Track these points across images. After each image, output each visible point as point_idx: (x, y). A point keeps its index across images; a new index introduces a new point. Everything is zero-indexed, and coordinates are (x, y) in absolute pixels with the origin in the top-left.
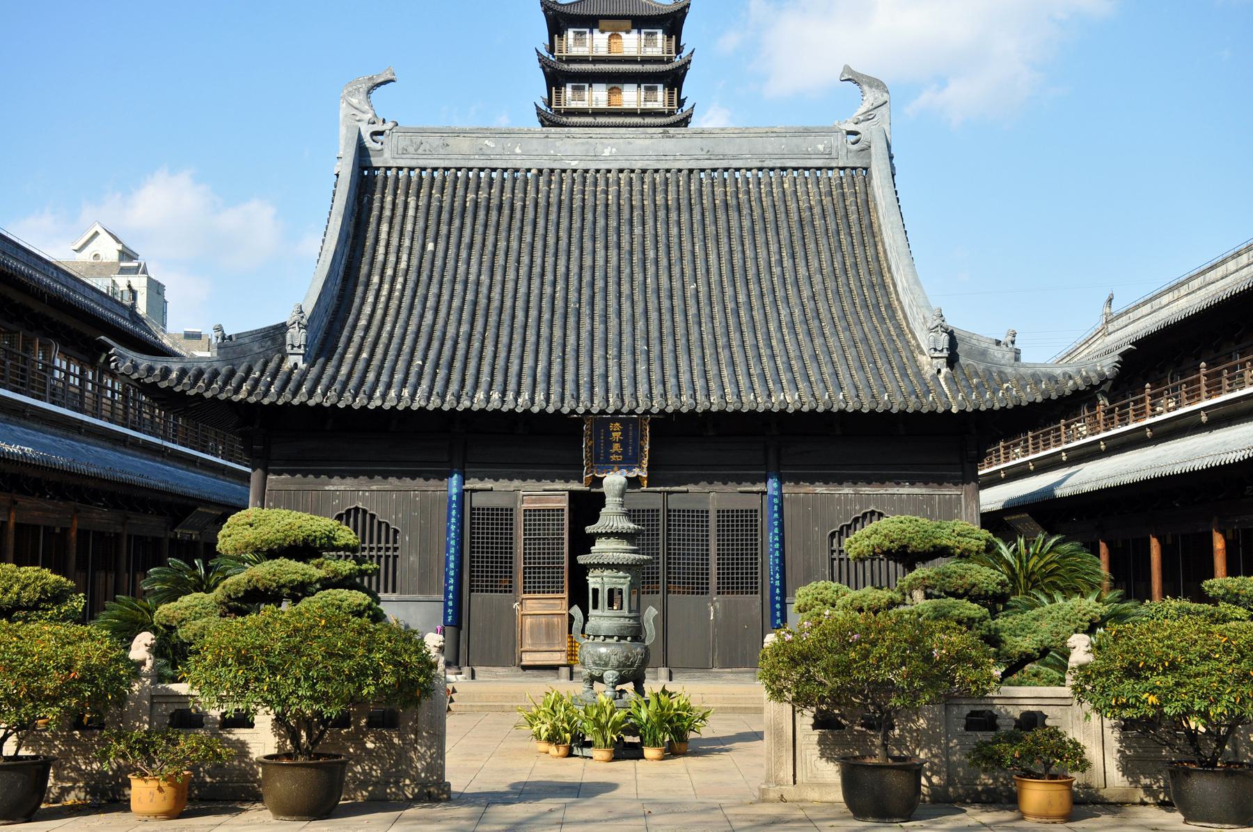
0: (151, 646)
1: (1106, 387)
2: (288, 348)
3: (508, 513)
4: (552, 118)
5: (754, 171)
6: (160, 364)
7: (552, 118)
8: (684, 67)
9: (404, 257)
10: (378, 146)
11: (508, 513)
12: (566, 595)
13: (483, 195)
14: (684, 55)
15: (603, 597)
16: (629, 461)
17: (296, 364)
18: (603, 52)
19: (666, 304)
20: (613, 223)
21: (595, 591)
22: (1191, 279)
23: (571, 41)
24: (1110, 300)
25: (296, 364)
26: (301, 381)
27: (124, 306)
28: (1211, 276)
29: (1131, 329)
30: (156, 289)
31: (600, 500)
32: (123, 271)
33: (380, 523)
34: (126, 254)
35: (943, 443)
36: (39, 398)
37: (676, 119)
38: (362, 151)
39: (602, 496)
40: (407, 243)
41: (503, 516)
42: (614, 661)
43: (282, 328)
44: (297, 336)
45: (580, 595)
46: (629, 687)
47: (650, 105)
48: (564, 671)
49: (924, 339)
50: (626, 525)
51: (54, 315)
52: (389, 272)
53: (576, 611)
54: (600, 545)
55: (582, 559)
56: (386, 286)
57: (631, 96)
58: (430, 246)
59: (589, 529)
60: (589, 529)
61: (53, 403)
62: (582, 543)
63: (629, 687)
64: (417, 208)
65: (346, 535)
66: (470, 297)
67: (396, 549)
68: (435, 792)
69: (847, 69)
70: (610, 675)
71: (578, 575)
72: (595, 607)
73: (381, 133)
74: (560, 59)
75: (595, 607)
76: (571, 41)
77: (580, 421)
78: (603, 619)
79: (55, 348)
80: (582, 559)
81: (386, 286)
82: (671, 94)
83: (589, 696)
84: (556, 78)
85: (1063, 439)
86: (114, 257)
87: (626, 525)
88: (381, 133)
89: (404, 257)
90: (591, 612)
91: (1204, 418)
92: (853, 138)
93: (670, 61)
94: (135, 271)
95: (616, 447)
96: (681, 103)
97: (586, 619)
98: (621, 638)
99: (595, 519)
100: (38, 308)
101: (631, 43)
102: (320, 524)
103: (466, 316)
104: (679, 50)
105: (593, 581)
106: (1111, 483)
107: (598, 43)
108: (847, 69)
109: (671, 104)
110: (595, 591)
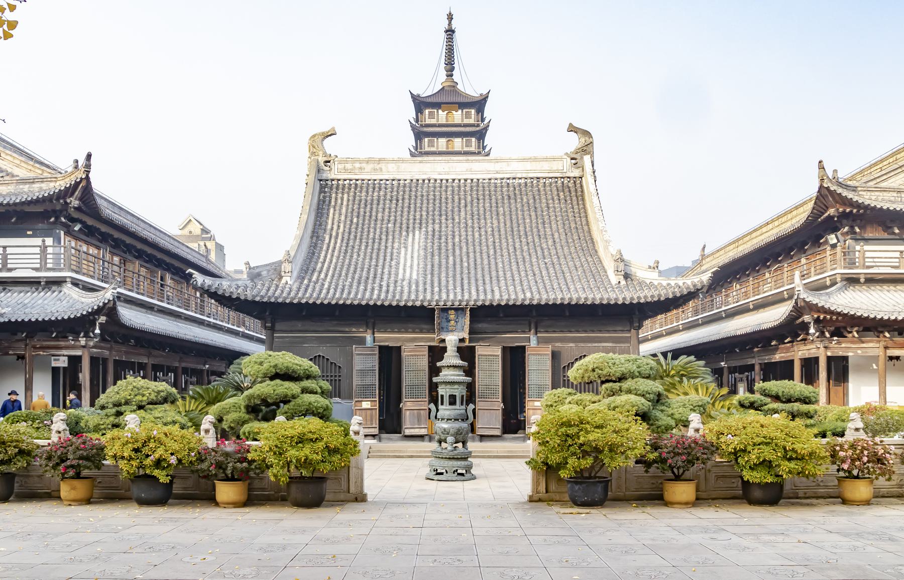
1: (705, 290)
2: (283, 274)
4: (418, 152)
6: (217, 281)
7: (418, 152)
8: (486, 128)
9: (342, 226)
10: (328, 168)
12: (427, 399)
13: (382, 193)
14: (485, 122)
15: (446, 400)
17: (287, 283)
18: (442, 120)
19: (478, 248)
20: (450, 206)
21: (442, 396)
22: (761, 227)
23: (427, 117)
24: (704, 247)
25: (287, 283)
26: (289, 288)
27: (203, 256)
28: (754, 235)
29: (762, 237)
30: (220, 248)
31: (444, 349)
32: (203, 239)
34: (205, 231)
35: (628, 316)
36: (152, 298)
37: (482, 151)
39: (446, 348)
40: (343, 218)
42: (452, 431)
45: (434, 399)
46: (460, 445)
47: (466, 121)
48: (427, 438)
49: (610, 266)
51: (168, 260)
52: (334, 234)
53: (432, 406)
54: (444, 372)
55: (435, 380)
56: (333, 241)
57: (458, 143)
58: (355, 220)
59: (438, 364)
60: (438, 364)
61: (138, 293)
62: (434, 370)
63: (460, 445)
64: (348, 200)
65: (315, 369)
66: (376, 246)
68: (360, 498)
69: (571, 125)
70: (450, 439)
71: (433, 387)
72: (442, 404)
73: (329, 162)
74: (422, 125)
75: (442, 404)
76: (427, 117)
77: (433, 310)
78: (445, 410)
79: (168, 276)
80: (435, 380)
81: (333, 241)
82: (479, 143)
83: (439, 450)
84: (419, 135)
85: (813, 273)
86: (198, 232)
87: (459, 362)
88: (329, 162)
89: (342, 226)
90: (440, 407)
91: (751, 307)
92: (573, 161)
93: (478, 126)
94: (210, 239)
96: (484, 148)
97: (438, 410)
98: (456, 420)
99: (442, 359)
100: (159, 255)
101: (457, 116)
102: (302, 363)
103: (374, 256)
104: (483, 120)
105: (441, 391)
106: (705, 340)
107: (442, 116)
108: (571, 125)
109: (479, 148)
110: (442, 396)
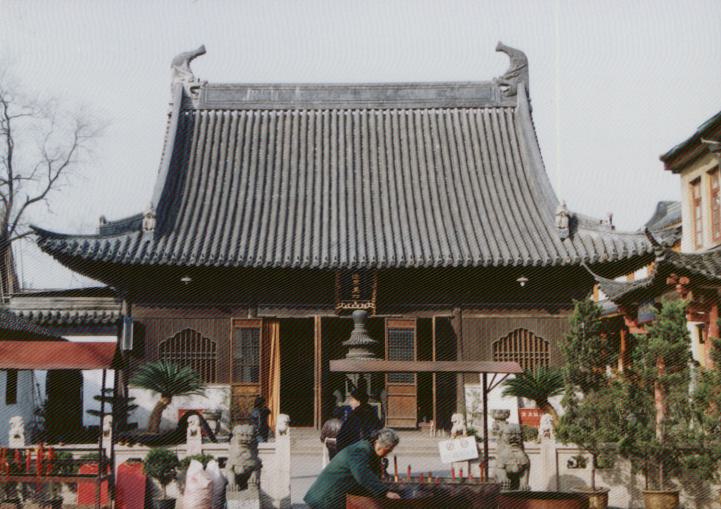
0: (608, 472)
3: (438, 359)
5: (433, 110)
11: (438, 359)
16: (364, 297)
26: (145, 246)
33: (204, 339)
38: (185, 99)
41: (420, 358)
43: (140, 217)
44: (151, 223)
50: (367, 340)
59: (345, 343)
67: (214, 355)
69: (500, 44)
73: (197, 88)
87: (367, 340)
88: (197, 88)
95: (356, 289)
99: (348, 336)
108: (500, 44)
